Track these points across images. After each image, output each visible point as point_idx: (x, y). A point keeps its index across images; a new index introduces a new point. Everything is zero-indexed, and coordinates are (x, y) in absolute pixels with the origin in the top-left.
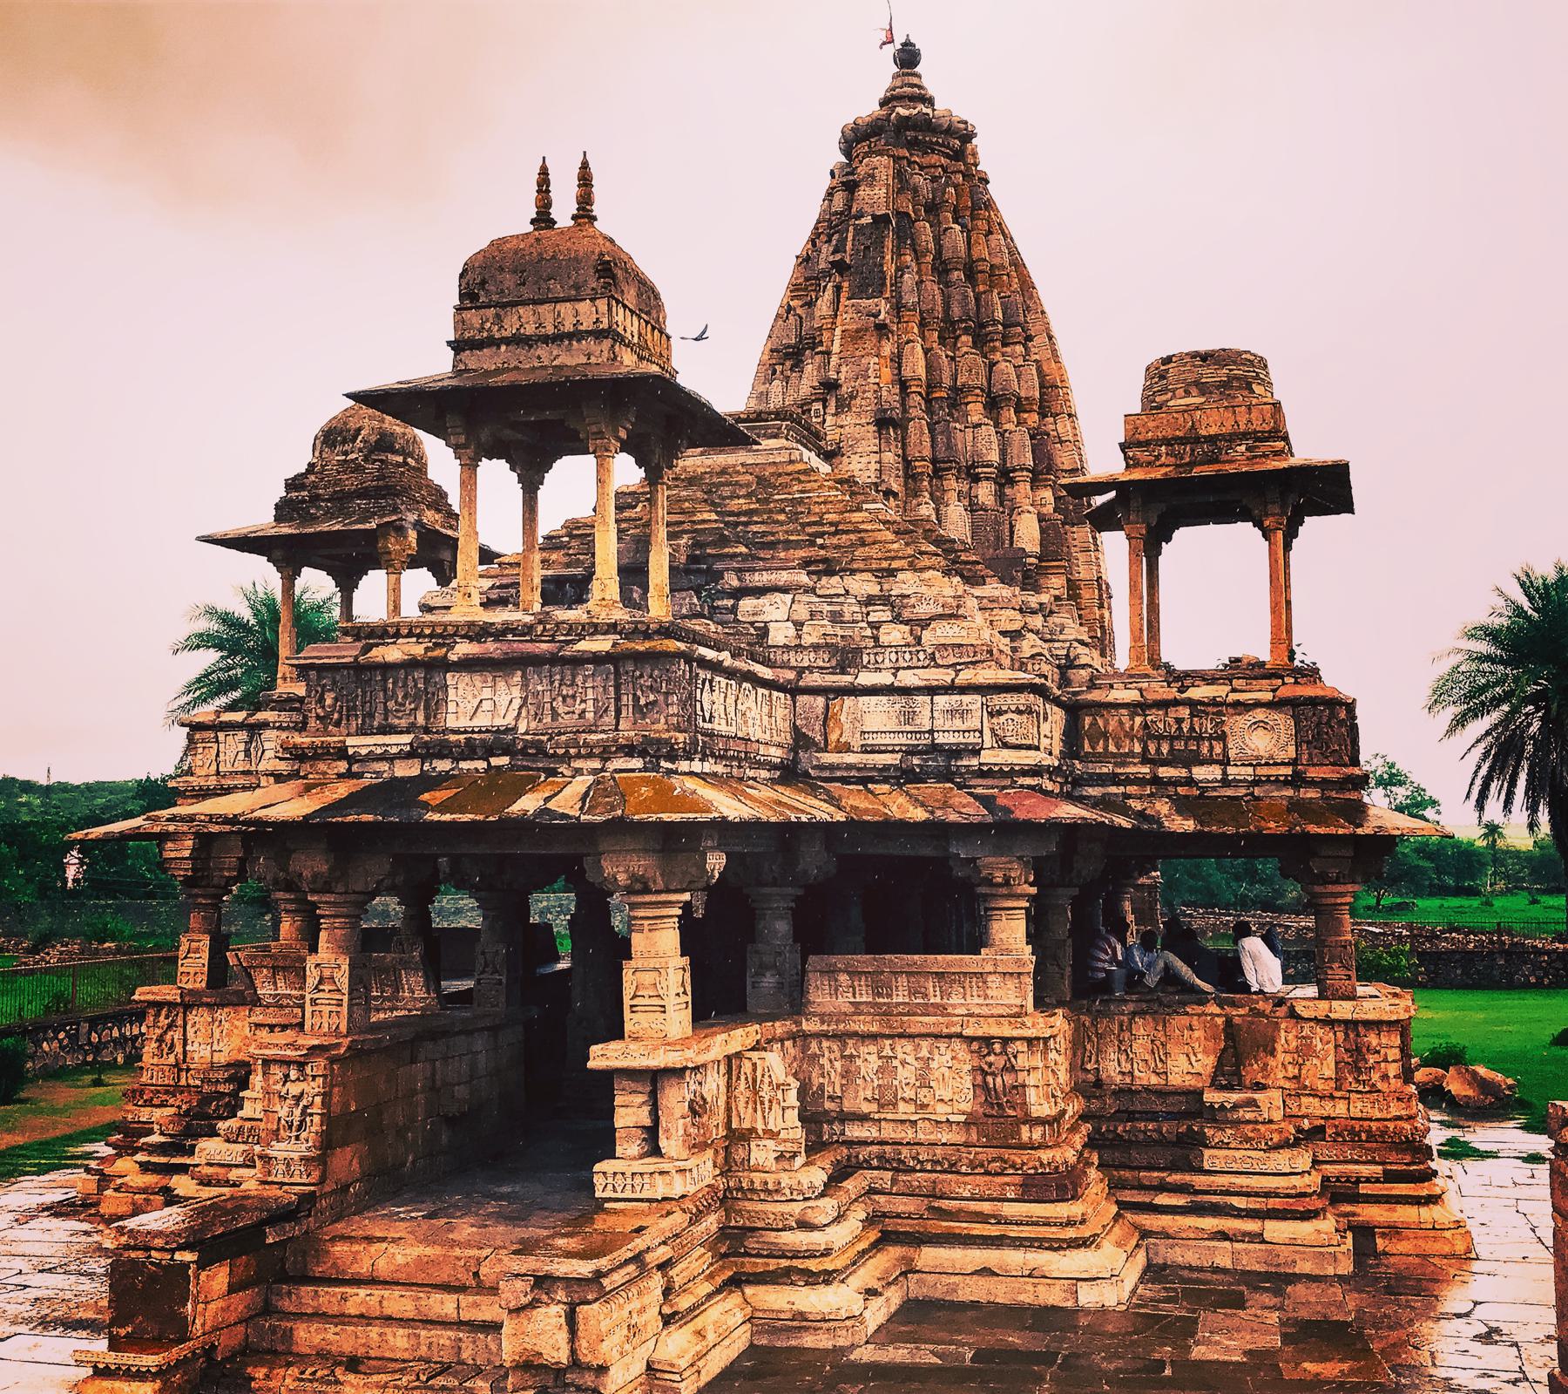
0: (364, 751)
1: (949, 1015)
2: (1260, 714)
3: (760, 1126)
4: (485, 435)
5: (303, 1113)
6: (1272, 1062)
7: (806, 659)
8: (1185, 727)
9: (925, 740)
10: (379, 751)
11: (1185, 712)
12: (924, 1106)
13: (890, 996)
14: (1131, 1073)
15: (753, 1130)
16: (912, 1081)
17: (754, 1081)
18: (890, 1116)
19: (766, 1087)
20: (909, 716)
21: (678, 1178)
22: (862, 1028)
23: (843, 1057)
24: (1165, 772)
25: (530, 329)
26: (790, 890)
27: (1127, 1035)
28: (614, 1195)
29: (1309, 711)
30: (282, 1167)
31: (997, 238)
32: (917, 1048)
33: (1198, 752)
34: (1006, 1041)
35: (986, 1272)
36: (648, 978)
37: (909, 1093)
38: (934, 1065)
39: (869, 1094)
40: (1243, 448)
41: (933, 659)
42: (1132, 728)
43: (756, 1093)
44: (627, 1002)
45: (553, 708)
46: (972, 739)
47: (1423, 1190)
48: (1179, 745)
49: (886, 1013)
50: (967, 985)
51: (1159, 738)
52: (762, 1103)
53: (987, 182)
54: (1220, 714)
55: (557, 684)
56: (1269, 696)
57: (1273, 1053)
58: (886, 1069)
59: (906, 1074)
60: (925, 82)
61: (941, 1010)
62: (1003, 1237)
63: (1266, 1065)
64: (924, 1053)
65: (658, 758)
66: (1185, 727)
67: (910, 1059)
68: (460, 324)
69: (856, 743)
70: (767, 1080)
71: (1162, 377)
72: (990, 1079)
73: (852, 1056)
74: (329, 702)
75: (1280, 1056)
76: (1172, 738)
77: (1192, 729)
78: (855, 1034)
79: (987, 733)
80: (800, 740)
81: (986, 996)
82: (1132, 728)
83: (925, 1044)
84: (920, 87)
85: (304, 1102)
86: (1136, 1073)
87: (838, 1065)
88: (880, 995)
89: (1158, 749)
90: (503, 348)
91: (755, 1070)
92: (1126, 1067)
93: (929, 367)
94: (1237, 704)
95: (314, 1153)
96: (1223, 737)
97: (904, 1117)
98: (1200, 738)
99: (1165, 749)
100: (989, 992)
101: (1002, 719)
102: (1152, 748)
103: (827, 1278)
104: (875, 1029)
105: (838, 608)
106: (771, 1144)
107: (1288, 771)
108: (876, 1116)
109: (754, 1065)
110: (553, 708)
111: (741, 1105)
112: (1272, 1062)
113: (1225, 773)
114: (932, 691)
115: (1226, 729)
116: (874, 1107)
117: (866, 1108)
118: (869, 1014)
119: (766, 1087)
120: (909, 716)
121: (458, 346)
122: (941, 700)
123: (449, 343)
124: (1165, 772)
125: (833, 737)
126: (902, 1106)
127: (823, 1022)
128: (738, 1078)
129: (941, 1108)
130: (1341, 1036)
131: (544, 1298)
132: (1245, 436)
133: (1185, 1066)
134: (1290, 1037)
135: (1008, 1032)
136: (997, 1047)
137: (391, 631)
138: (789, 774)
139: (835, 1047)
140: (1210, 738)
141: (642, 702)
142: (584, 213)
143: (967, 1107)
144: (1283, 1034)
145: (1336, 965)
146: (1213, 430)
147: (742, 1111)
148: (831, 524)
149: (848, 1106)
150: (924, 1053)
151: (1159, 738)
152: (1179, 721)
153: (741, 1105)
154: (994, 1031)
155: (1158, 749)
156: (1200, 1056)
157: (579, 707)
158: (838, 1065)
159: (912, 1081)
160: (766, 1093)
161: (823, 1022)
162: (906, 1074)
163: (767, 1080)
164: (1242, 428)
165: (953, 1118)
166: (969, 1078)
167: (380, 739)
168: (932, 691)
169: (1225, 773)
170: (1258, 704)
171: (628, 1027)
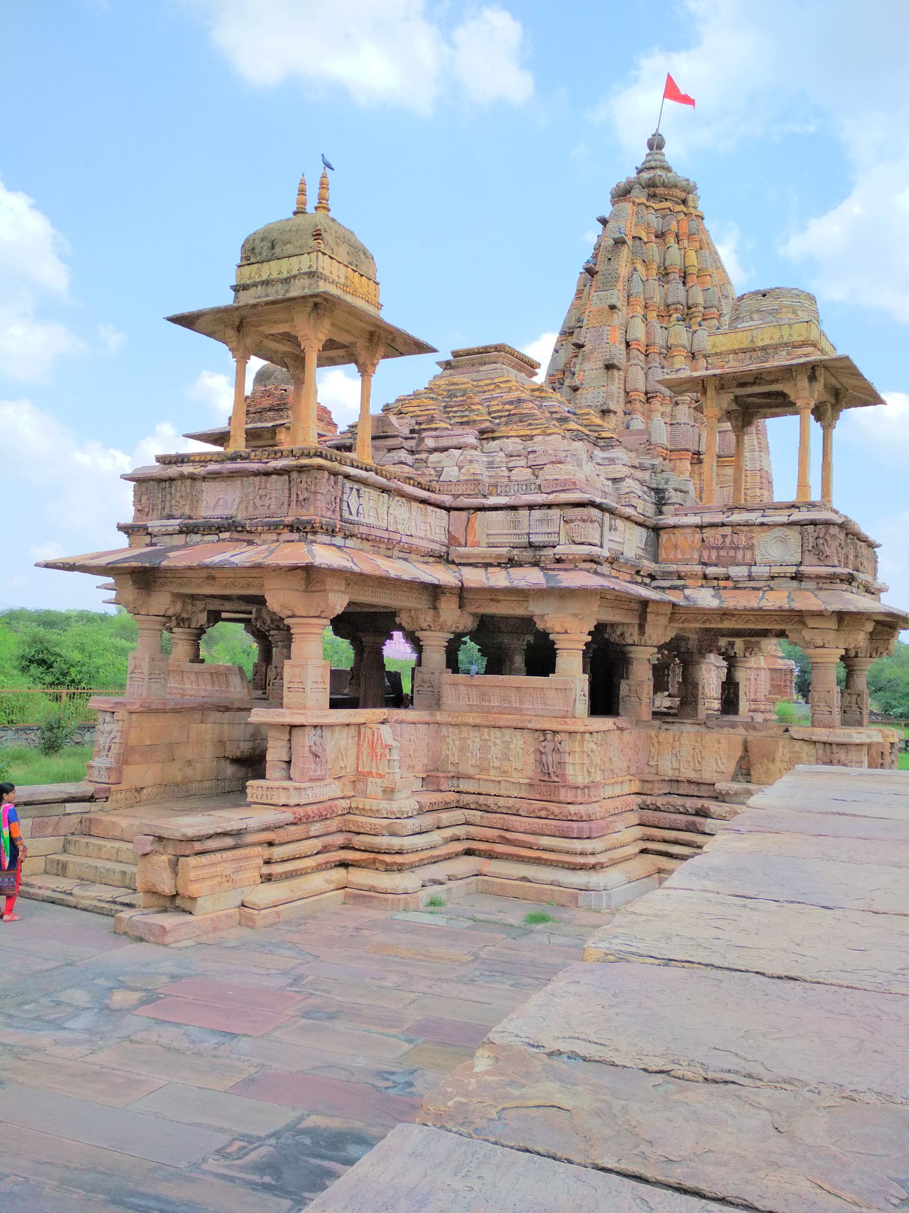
0: (156, 530)
1: (524, 715)
2: (777, 532)
3: (374, 771)
4: (249, 341)
5: (111, 742)
6: (772, 767)
7: (460, 489)
8: (728, 540)
9: (524, 540)
10: (164, 529)
11: (728, 530)
12: (505, 772)
13: (489, 701)
14: (679, 769)
15: (370, 773)
16: (499, 756)
17: (373, 742)
18: (485, 777)
19: (379, 747)
20: (516, 524)
21: (293, 792)
22: (471, 721)
23: (460, 738)
24: (711, 570)
25: (275, 276)
26: (441, 634)
27: (677, 744)
28: (256, 800)
29: (811, 528)
30: (97, 772)
31: (705, 252)
32: (503, 735)
33: (734, 557)
34: (555, 732)
35: (524, 879)
36: (297, 670)
37: (497, 764)
38: (513, 746)
39: (474, 762)
40: (784, 353)
41: (540, 489)
42: (693, 542)
43: (373, 750)
44: (286, 685)
45: (254, 503)
46: (553, 539)
47: (649, 815)
48: (723, 553)
49: (488, 711)
50: (534, 696)
51: (711, 548)
52: (376, 756)
53: (703, 219)
54: (751, 531)
55: (257, 488)
56: (785, 519)
57: (773, 761)
58: (485, 747)
59: (495, 751)
60: (667, 158)
61: (519, 711)
62: (539, 859)
63: (768, 769)
64: (507, 738)
65: (307, 533)
66: (728, 540)
67: (498, 742)
68: (239, 276)
69: (484, 541)
70: (379, 742)
71: (737, 310)
72: (544, 757)
73: (465, 738)
74: (143, 501)
75: (778, 763)
76: (718, 548)
77: (732, 542)
78: (467, 725)
79: (562, 534)
80: (452, 540)
81: (546, 704)
82: (693, 542)
83: (508, 732)
84: (664, 161)
85: (112, 736)
86: (682, 769)
87: (457, 743)
88: (483, 700)
89: (709, 556)
90: (259, 287)
91: (373, 735)
92: (676, 765)
93: (648, 333)
94: (762, 524)
95: (114, 765)
96: (751, 548)
97: (493, 778)
98: (737, 548)
99: (714, 555)
100: (548, 701)
101: (572, 525)
102: (705, 554)
103: (400, 868)
104: (478, 721)
105: (491, 459)
106: (379, 780)
107: (793, 569)
108: (477, 777)
109: (373, 732)
110: (254, 503)
111: (365, 756)
112: (772, 767)
113: (750, 571)
114: (531, 507)
115: (754, 541)
116: (476, 771)
117: (472, 771)
118: (478, 712)
119: (379, 747)
120: (516, 524)
121: (236, 289)
122: (537, 514)
123: (232, 287)
124: (711, 570)
125: (470, 539)
126: (492, 772)
127: (449, 715)
128: (364, 740)
129: (515, 774)
130: (821, 752)
131: (161, 850)
132: (786, 345)
133: (715, 767)
134: (786, 751)
135: (555, 727)
136: (549, 737)
137: (180, 460)
138: (444, 559)
139: (456, 732)
140: (744, 548)
141: (301, 498)
142: (323, 205)
143: (530, 774)
144: (781, 749)
145: (822, 704)
146: (767, 342)
147: (365, 759)
148: (507, 410)
149: (462, 769)
150: (507, 738)
151: (711, 548)
152: (724, 536)
153: (365, 756)
154: (546, 726)
155: (709, 556)
156: (724, 761)
157: (267, 502)
158: (457, 743)
159: (499, 756)
160: (379, 751)
161: (449, 715)
162: (495, 751)
163: (379, 742)
164: (785, 339)
165: (522, 781)
166: (533, 756)
167: (165, 522)
168: (531, 507)
169: (750, 571)
170: (776, 525)
171: (285, 700)
